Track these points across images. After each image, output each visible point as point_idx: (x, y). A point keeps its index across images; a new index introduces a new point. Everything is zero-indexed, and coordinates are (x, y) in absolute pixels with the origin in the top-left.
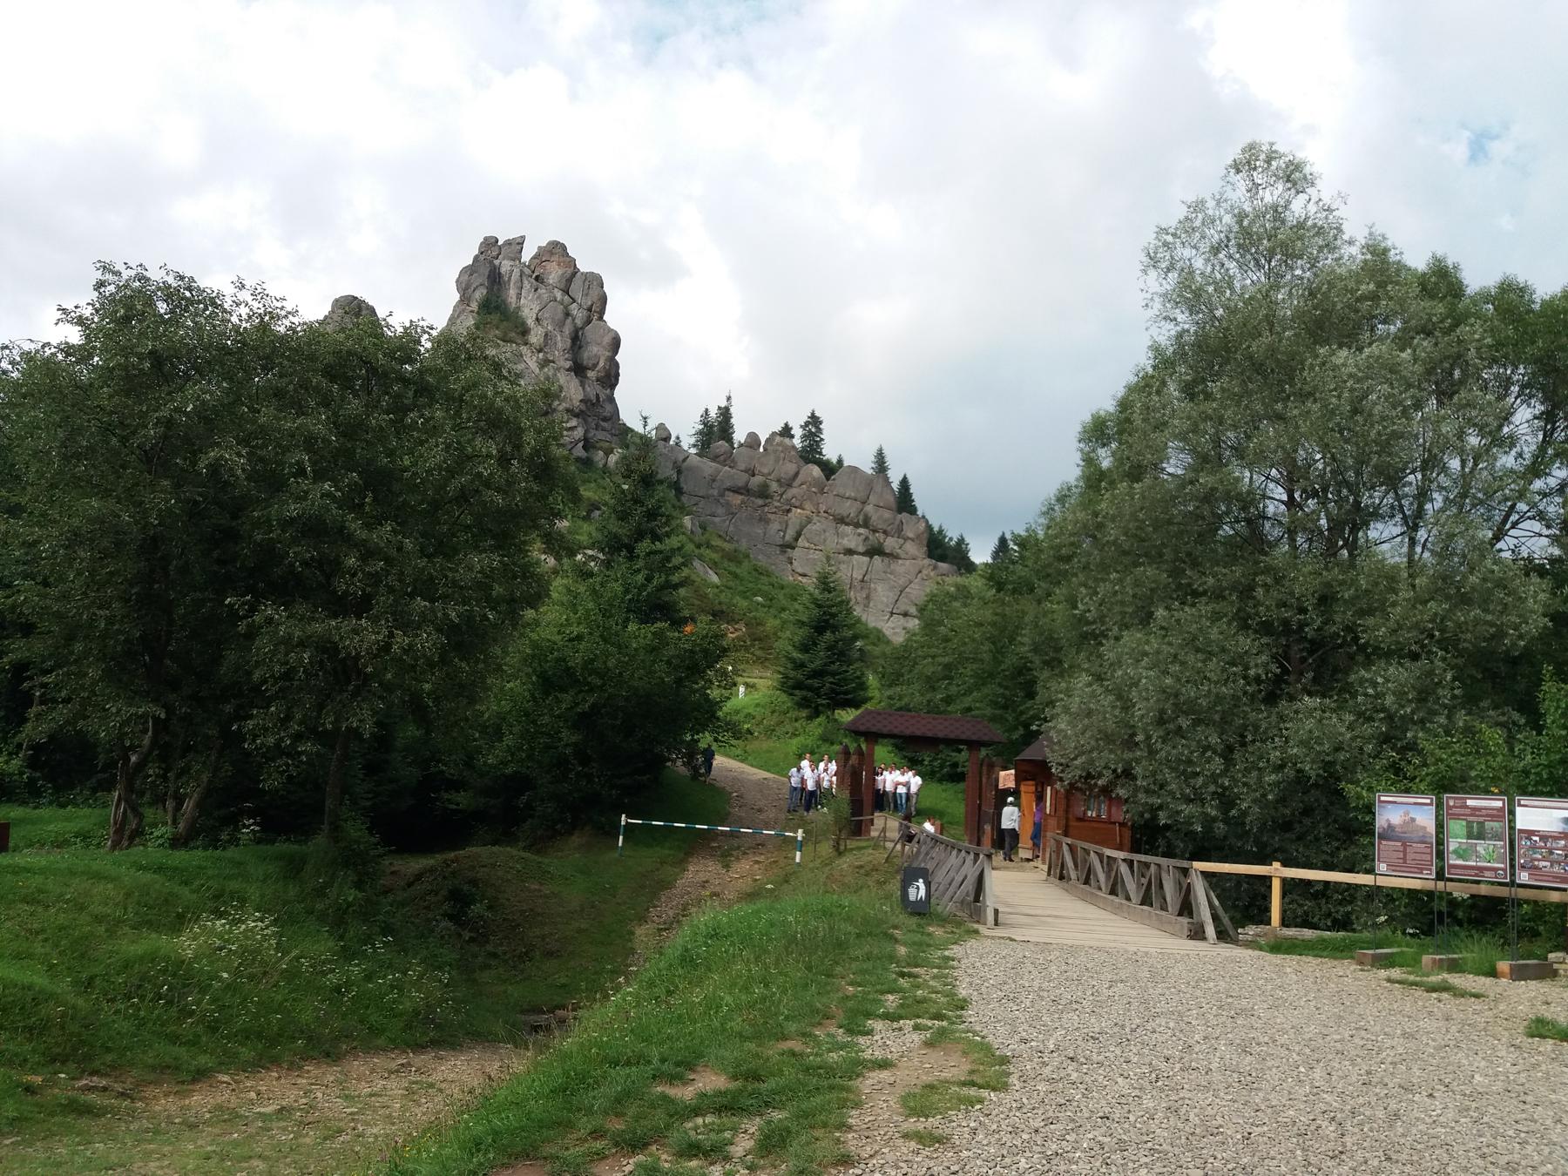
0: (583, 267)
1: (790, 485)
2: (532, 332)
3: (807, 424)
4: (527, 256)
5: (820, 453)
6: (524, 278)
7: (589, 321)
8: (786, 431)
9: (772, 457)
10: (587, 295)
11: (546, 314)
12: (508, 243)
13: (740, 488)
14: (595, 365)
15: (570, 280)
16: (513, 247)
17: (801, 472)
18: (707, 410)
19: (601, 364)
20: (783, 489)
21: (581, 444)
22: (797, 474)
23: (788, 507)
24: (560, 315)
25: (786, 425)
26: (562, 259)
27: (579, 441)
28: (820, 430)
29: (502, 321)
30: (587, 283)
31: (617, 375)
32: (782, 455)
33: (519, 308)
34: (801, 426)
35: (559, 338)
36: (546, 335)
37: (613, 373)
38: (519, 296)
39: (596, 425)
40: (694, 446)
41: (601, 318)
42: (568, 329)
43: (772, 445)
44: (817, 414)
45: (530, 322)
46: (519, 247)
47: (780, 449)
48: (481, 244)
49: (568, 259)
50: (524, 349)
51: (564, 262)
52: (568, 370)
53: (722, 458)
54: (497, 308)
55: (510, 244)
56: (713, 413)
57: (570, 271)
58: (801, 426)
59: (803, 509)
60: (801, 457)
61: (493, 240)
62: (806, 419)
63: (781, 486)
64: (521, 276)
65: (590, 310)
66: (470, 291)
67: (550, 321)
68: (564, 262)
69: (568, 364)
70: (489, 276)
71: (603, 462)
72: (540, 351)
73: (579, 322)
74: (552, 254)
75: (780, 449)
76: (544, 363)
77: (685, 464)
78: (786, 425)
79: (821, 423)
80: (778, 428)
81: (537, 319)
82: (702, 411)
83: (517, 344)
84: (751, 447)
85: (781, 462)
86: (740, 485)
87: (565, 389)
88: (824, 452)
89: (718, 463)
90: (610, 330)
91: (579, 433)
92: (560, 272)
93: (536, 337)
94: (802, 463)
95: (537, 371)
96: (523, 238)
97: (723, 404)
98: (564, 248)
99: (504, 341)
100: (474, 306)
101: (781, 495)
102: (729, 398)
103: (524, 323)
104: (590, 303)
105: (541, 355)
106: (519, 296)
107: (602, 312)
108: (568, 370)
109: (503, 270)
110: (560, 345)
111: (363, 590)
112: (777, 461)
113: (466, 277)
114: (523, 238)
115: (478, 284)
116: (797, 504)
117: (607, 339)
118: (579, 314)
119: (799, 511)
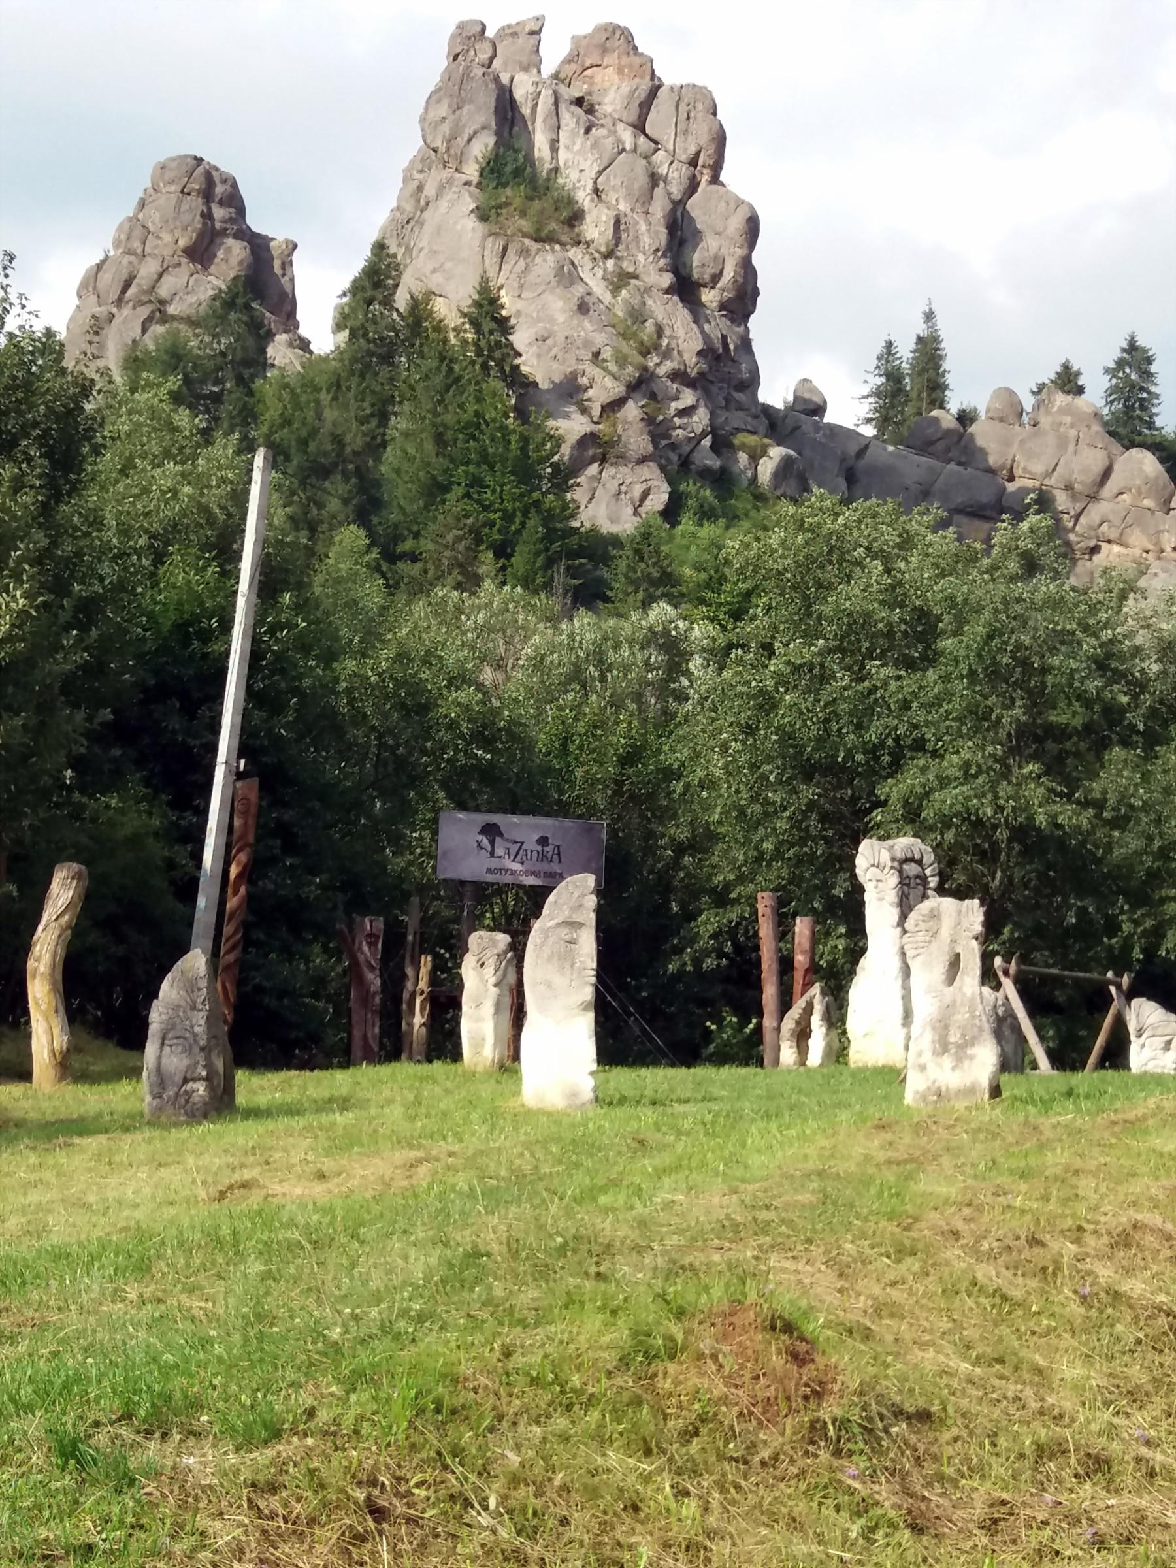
0: (670, 74)
1: (1093, 497)
2: (588, 218)
3: (1120, 364)
4: (553, 52)
5: (1151, 425)
6: (563, 107)
7: (692, 187)
8: (1068, 381)
9: (1051, 439)
10: (686, 132)
11: (612, 181)
12: (511, 32)
13: (983, 507)
14: (716, 278)
15: (646, 105)
16: (520, 41)
17: (1116, 467)
18: (890, 344)
19: (729, 274)
20: (1079, 506)
21: (707, 442)
22: (1107, 474)
23: (1092, 543)
24: (642, 180)
25: (1066, 367)
26: (625, 60)
27: (704, 435)
28: (1147, 375)
29: (531, 199)
30: (683, 108)
31: (756, 293)
32: (1073, 433)
33: (556, 170)
34: (1107, 371)
35: (643, 227)
36: (617, 223)
37: (750, 289)
38: (554, 149)
39: (727, 400)
40: (868, 421)
41: (715, 179)
42: (659, 208)
43: (1048, 412)
44: (1141, 342)
45: (583, 197)
46: (533, 40)
47: (1068, 420)
48: (453, 37)
49: (637, 61)
50: (576, 254)
51: (631, 66)
52: (667, 292)
53: (940, 446)
54: (517, 173)
55: (515, 34)
56: (905, 351)
57: (645, 85)
58: (1107, 371)
59: (1127, 546)
60: (1112, 434)
61: (478, 29)
62: (1117, 354)
63: (1074, 497)
64: (556, 103)
65: (693, 162)
66: (461, 141)
67: (622, 192)
68: (631, 66)
69: (667, 279)
70: (497, 111)
71: (749, 474)
72: (608, 255)
73: (676, 191)
74: (605, 51)
75: (1068, 420)
76: (620, 281)
77: (862, 463)
78: (1066, 367)
79: (1149, 361)
80: (1048, 373)
81: (597, 191)
82: (878, 348)
83: (563, 244)
84: (1002, 420)
85: (1071, 447)
86: (985, 499)
87: (668, 332)
88: (1159, 421)
89: (932, 455)
90: (740, 202)
91: (701, 419)
92: (626, 88)
93: (596, 228)
94: (1116, 447)
95: (607, 298)
96: (540, 19)
97: (921, 329)
98: (627, 37)
99: (537, 240)
100: (472, 171)
101: (1077, 517)
102: (929, 316)
103: (571, 201)
104: (693, 149)
105: (610, 263)
106: (554, 149)
107: (717, 167)
108: (667, 292)
109: (519, 94)
110: (646, 241)
111: (849, 755)
112: (1062, 444)
113: (443, 110)
114: (540, 19)
115: (476, 127)
116: (1113, 535)
117: (736, 223)
118: (676, 177)
119: (1116, 549)
